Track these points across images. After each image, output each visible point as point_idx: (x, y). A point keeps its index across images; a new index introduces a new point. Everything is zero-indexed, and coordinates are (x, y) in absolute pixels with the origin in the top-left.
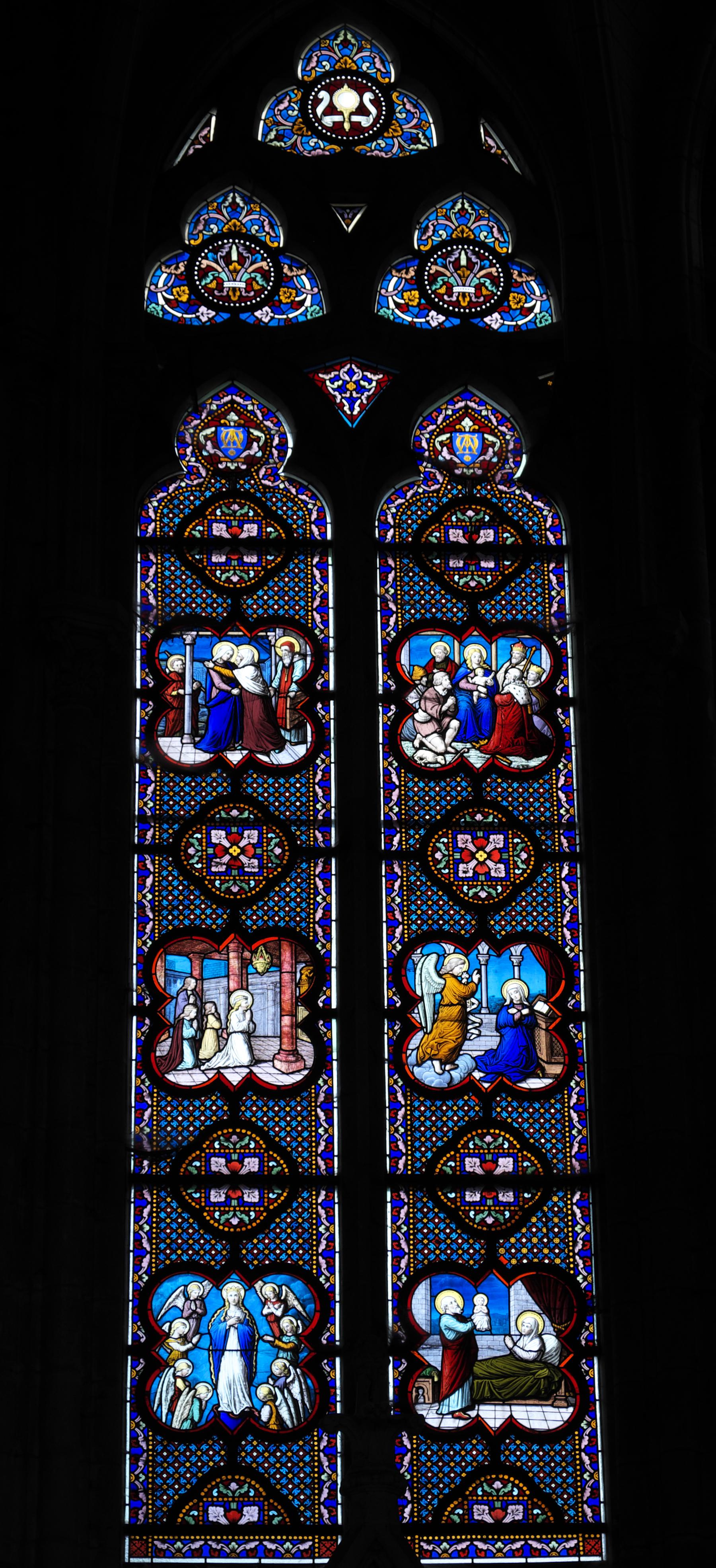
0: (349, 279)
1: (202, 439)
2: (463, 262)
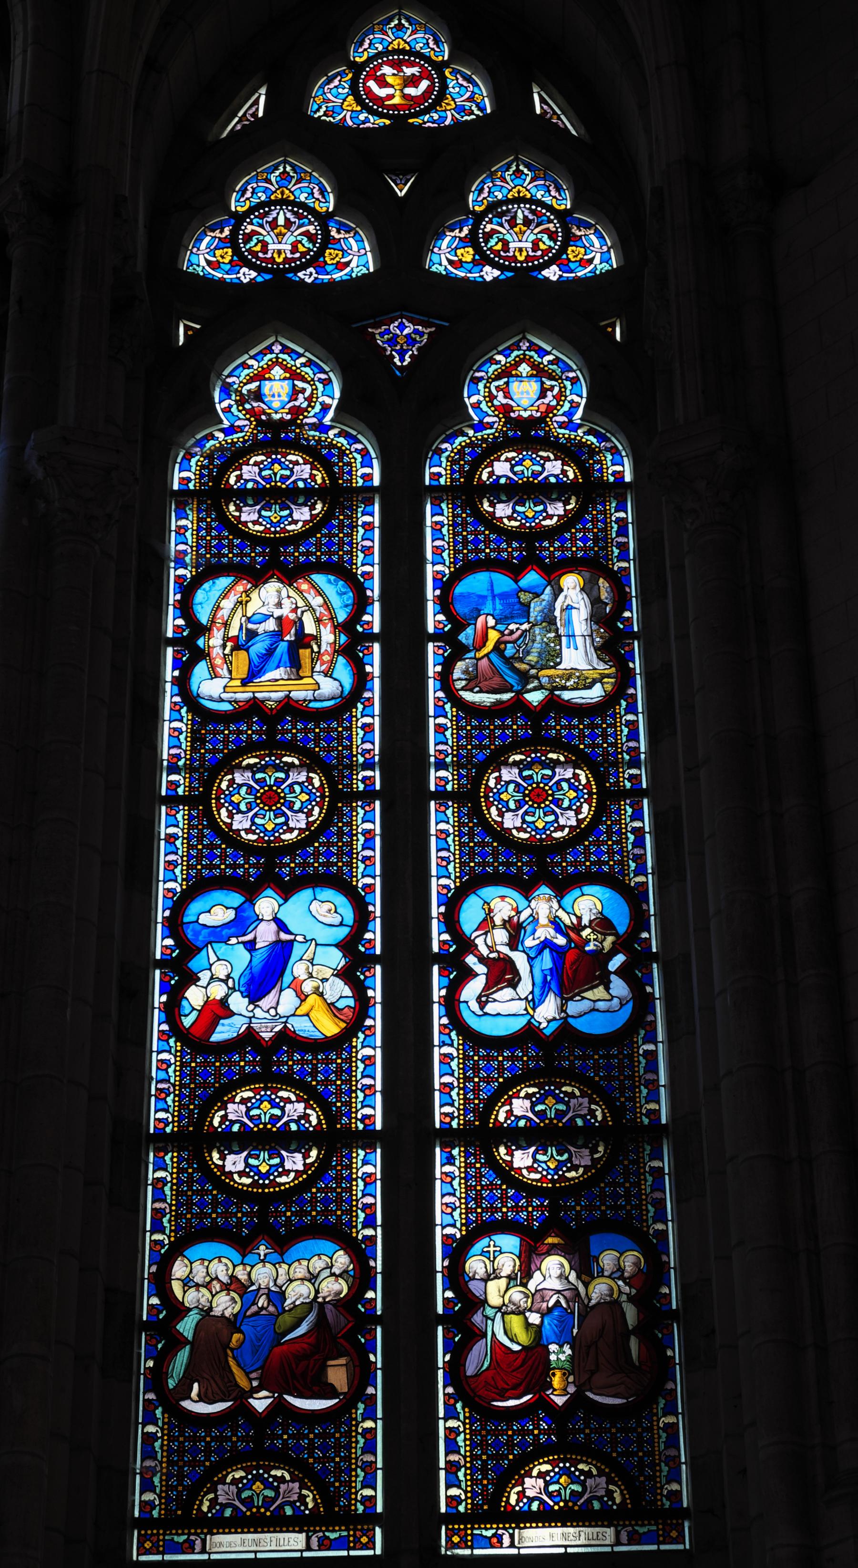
0: (402, 239)
2: (281, 221)
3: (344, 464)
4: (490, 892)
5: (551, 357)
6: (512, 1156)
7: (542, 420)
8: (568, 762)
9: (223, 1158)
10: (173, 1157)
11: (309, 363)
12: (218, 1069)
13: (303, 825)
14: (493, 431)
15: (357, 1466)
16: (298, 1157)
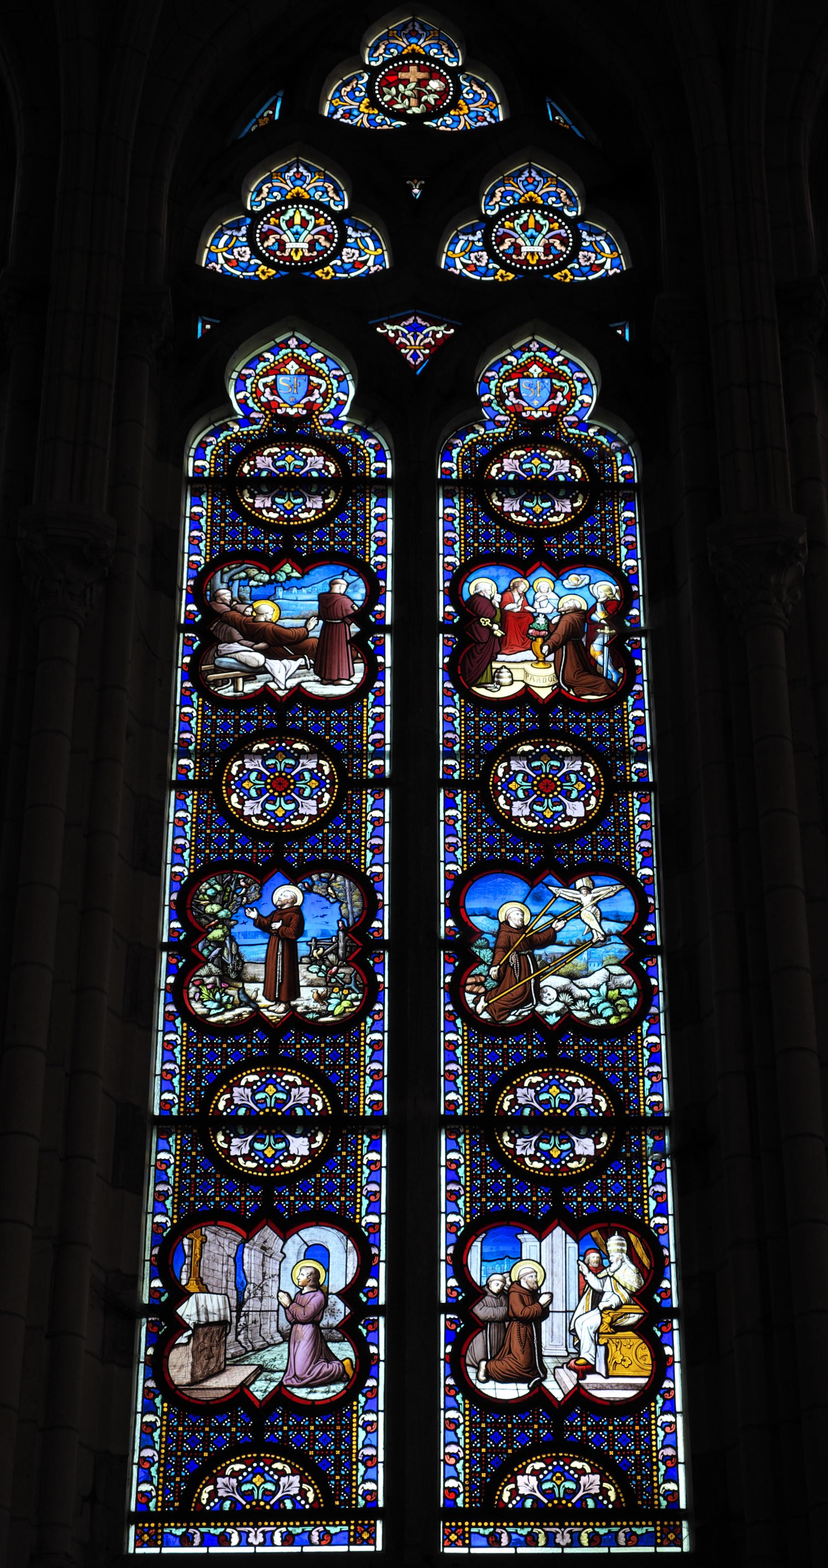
0: (414, 240)
1: (505, 390)
5: (560, 358)
7: (308, 417)
10: (176, 1139)
11: (566, 362)
14: (504, 430)
16: (588, 1142)
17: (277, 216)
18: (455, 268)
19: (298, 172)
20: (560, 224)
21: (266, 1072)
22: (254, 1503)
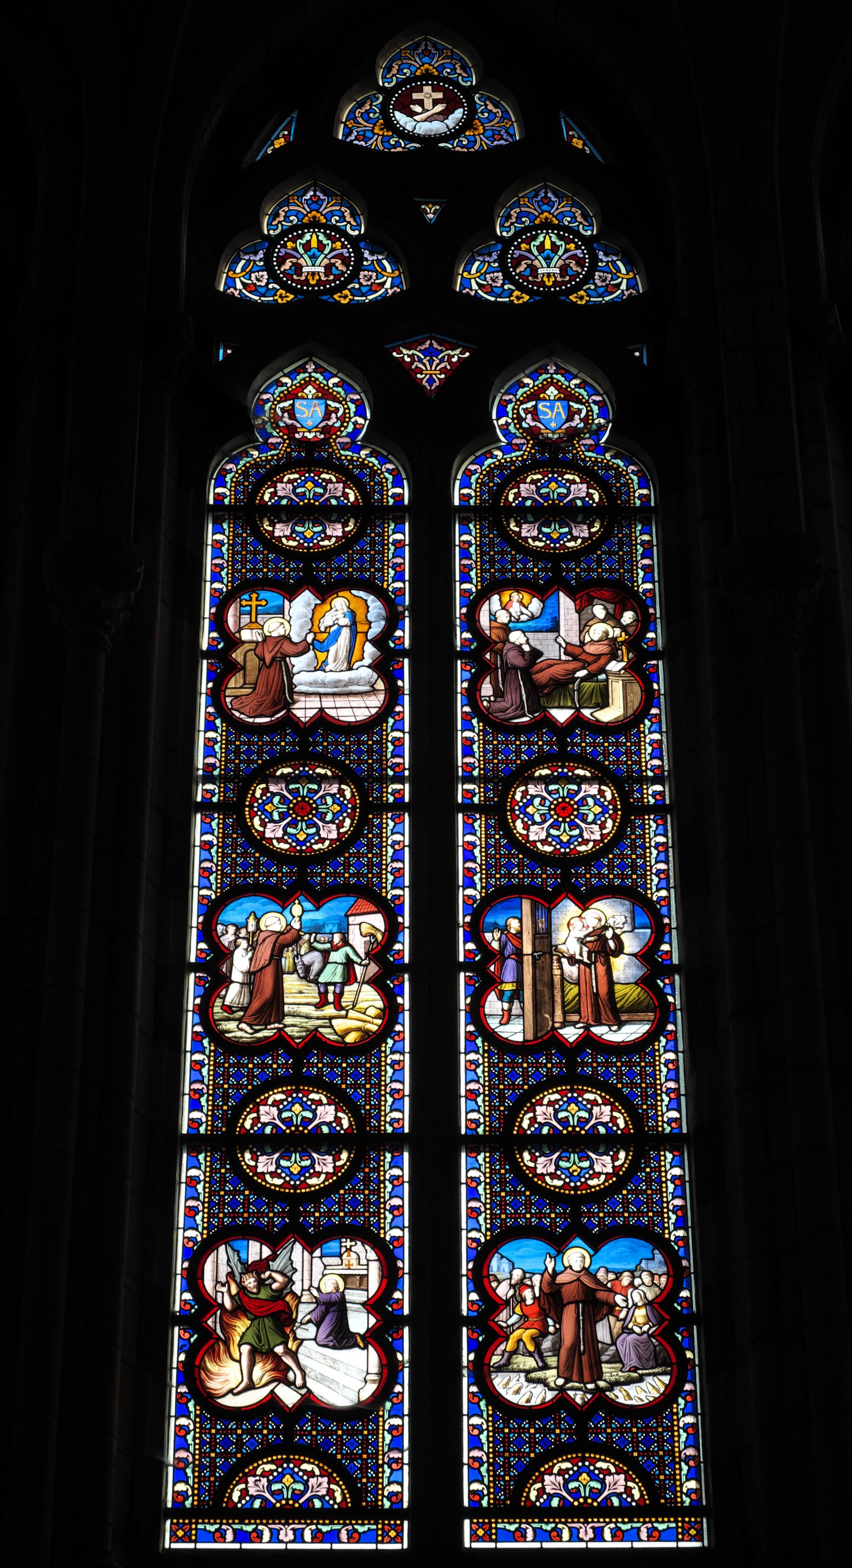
0: (429, 260)
3: (376, 484)
4: (249, 904)
6: (256, 1160)
8: (335, 779)
9: (255, 1158)
10: (485, 1157)
11: (583, 385)
12: (525, 1070)
13: (597, 837)
15: (681, 1460)
16: (607, 1159)
17: (528, 241)
18: (236, 289)
19: (315, 195)
20: (343, 243)
21: (292, 1091)
22: (581, 1500)
